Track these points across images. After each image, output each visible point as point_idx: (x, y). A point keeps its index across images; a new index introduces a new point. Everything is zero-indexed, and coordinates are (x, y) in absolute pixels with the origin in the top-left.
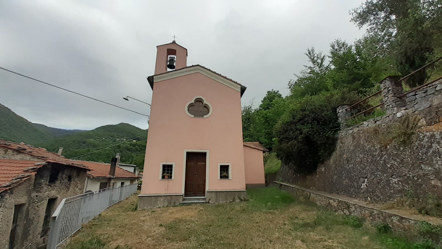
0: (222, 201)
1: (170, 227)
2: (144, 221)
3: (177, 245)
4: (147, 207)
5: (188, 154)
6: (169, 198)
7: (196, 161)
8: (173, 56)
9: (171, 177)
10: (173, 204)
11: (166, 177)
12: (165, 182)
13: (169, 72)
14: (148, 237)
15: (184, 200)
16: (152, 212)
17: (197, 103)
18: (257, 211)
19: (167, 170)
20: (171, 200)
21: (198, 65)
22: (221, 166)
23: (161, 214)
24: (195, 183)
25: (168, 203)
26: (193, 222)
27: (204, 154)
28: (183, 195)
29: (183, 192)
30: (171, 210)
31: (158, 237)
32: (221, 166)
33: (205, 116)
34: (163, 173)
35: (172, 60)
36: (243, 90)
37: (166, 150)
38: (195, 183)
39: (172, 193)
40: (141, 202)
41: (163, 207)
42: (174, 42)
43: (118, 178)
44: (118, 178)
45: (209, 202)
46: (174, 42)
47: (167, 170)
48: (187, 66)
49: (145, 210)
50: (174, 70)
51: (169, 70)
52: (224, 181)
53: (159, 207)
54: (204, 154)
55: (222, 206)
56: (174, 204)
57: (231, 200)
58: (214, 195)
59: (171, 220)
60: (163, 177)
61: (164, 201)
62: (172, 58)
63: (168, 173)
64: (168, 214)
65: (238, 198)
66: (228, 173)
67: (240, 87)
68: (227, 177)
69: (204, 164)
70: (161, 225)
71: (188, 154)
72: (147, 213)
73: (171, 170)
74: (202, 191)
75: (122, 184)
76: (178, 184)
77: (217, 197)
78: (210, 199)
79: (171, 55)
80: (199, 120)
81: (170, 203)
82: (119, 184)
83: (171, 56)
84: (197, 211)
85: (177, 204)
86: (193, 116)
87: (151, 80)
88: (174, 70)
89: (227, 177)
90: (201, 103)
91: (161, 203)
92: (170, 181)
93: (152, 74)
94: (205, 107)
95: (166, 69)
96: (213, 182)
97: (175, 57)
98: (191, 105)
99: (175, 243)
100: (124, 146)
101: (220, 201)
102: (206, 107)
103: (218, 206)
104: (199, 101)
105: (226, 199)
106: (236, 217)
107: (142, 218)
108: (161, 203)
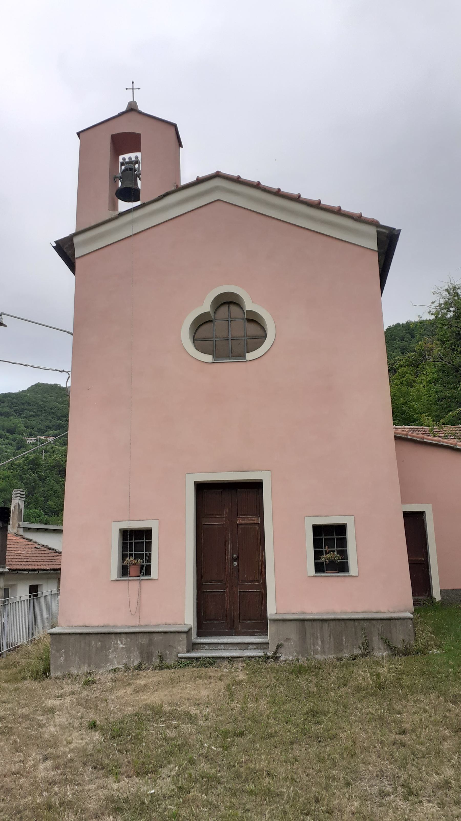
0: (324, 653)
1: (117, 733)
2: (52, 710)
3: (115, 786)
4: (79, 667)
5: (202, 488)
6: (143, 640)
7: (229, 511)
8: (133, 155)
9: (148, 571)
10: (156, 661)
11: (133, 570)
12: (132, 586)
13: (122, 214)
14: (46, 759)
15: (193, 646)
16: (86, 683)
17: (224, 309)
18: (427, 691)
19: (136, 545)
20: (152, 648)
21: (218, 175)
22: (422, 514)
23: (111, 690)
24: (230, 587)
25: (141, 654)
26: (192, 719)
27: (256, 486)
28: (188, 632)
29: (189, 619)
30: (149, 677)
31: (71, 761)
32: (422, 514)
33: (249, 356)
34: (124, 557)
35: (131, 172)
36: (388, 242)
37: (127, 478)
38: (230, 587)
39: (154, 622)
40: (58, 651)
41: (127, 669)
42: (132, 109)
43: (18, 573)
44: (18, 573)
45: (276, 658)
46: (132, 109)
47: (136, 545)
48: (184, 181)
49: (69, 675)
50: (138, 203)
51: (123, 206)
52: (332, 582)
53: (115, 670)
54: (256, 486)
55: (315, 669)
56: (161, 661)
57: (357, 651)
58: (292, 632)
59: (130, 710)
60: (125, 571)
61: (128, 651)
62: (130, 162)
63: (141, 556)
64: (129, 690)
65: (381, 645)
66: (344, 553)
67: (373, 231)
68: (342, 567)
69: (256, 520)
70: (93, 726)
71: (202, 488)
72: (67, 689)
73: (149, 546)
74: (257, 620)
75: (34, 589)
76: (171, 595)
77: (303, 637)
78: (279, 646)
79: (125, 154)
80: (230, 370)
81: (146, 656)
82: (22, 591)
83: (127, 156)
84: (221, 684)
85: (170, 661)
86: (209, 358)
87: (65, 249)
88: (138, 203)
89: (342, 567)
90: (234, 308)
91: (119, 656)
92: (147, 585)
93: (67, 228)
94: (250, 321)
95: (114, 206)
96: (290, 584)
97: (139, 154)
98: (201, 322)
99: (112, 778)
100: (50, 460)
101: (315, 652)
102: (254, 319)
103: (301, 670)
104: (227, 301)
105: (339, 648)
106: (341, 709)
107: (50, 703)
108: (119, 656)
